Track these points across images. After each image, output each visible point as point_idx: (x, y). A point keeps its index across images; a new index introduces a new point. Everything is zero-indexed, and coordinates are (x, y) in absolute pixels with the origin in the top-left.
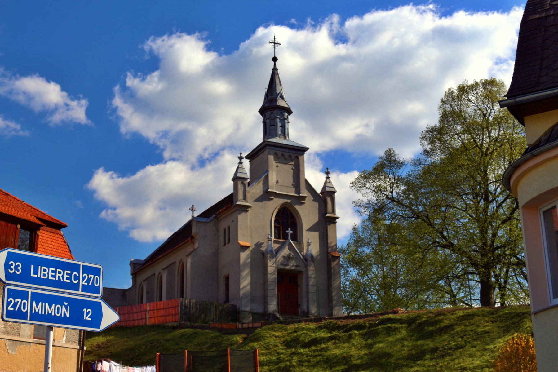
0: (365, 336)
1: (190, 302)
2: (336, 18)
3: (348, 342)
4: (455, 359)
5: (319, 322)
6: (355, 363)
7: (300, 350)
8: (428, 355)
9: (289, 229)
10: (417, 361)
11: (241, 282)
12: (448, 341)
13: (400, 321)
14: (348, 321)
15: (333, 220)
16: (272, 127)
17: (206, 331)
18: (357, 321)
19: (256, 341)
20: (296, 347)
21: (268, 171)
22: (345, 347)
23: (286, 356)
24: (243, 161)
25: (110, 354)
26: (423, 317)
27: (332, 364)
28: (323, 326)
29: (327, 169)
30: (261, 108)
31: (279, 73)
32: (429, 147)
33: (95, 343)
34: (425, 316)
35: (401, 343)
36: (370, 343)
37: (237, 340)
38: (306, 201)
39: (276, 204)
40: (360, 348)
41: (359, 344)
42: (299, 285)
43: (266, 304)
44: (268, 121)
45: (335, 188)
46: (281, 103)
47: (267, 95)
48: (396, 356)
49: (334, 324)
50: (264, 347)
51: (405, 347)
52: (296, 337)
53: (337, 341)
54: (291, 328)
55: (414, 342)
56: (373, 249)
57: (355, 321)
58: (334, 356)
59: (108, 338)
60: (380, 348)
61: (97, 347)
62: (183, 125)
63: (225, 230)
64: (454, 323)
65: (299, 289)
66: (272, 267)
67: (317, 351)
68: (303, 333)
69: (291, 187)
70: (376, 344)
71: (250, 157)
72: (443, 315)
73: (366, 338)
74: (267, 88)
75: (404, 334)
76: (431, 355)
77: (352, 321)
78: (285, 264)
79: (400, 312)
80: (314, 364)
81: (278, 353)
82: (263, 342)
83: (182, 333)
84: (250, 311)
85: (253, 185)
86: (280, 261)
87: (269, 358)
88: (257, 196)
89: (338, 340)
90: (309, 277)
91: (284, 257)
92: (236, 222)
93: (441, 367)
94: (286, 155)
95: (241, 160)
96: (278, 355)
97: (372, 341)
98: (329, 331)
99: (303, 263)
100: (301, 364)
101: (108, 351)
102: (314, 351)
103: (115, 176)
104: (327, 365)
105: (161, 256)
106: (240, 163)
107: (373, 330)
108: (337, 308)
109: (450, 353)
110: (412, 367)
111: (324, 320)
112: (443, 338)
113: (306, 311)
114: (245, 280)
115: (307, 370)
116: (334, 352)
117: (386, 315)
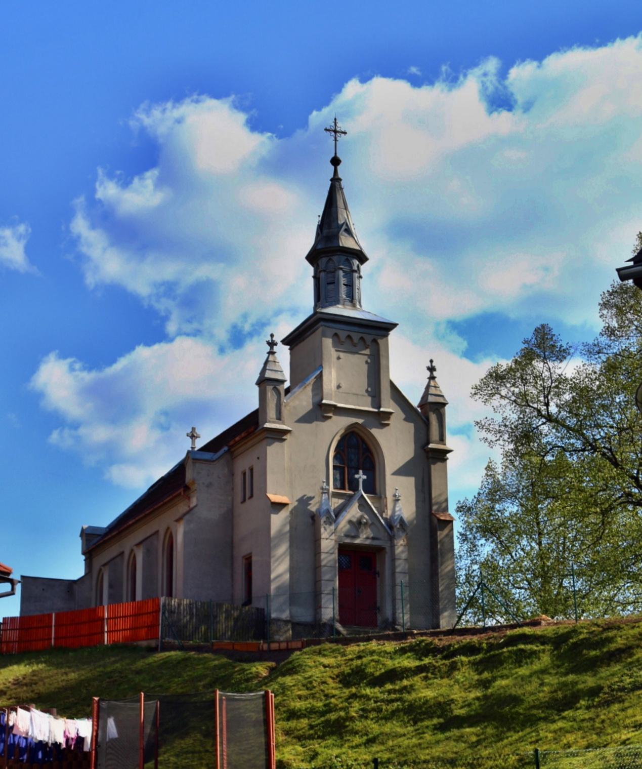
0: (479, 667)
1: (179, 605)
2: (492, 65)
3: (448, 677)
4: (629, 707)
5: (400, 640)
6: (458, 714)
7: (365, 690)
8: (584, 700)
9: (361, 472)
10: (563, 710)
11: (272, 567)
12: (619, 675)
13: (542, 640)
14: (452, 639)
15: (441, 455)
16: (331, 287)
17: (206, 655)
18: (467, 639)
19: (290, 674)
20: (359, 684)
21: (321, 366)
22: (443, 686)
23: (340, 700)
24: (275, 349)
25: (36, 696)
26: (581, 633)
27: (418, 716)
28: (407, 648)
29: (431, 361)
30: (310, 252)
31: (343, 187)
32: (614, 324)
33: (12, 678)
34: (585, 631)
35: (539, 678)
36: (486, 678)
37: (258, 672)
38: (392, 421)
39: (337, 426)
40: (469, 688)
41: (467, 679)
42: (378, 573)
43: (317, 606)
44: (322, 275)
45: (445, 396)
46: (346, 242)
47: (320, 227)
48: (529, 702)
49: (427, 644)
50: (304, 686)
51: (546, 686)
52: (360, 667)
53: (429, 675)
54: (352, 651)
55: (561, 677)
56: (522, 505)
57: (464, 639)
58: (422, 701)
59: (35, 667)
60: (502, 687)
61: (14, 684)
62: (203, 271)
63: (244, 474)
64: (635, 643)
65: (378, 579)
66: (328, 542)
67: (395, 691)
68: (373, 660)
69: (363, 395)
70: (497, 680)
71: (292, 340)
72: (616, 629)
73: (480, 670)
74: (321, 215)
75: (546, 664)
76: (588, 700)
77: (458, 638)
78: (353, 534)
79: (543, 623)
80: (387, 715)
81: (327, 696)
82: (301, 675)
83: (163, 659)
84: (288, 619)
85: (294, 393)
86: (344, 529)
87: (310, 703)
88: (302, 413)
89: (432, 673)
90: (397, 557)
91: (350, 522)
92: (263, 459)
93: (603, 721)
94: (356, 337)
95: (272, 348)
96: (326, 700)
97: (490, 675)
98: (418, 657)
99: (386, 534)
100: (365, 715)
101: (32, 691)
102: (389, 692)
103: (77, 366)
104: (410, 717)
105: (134, 521)
106: (271, 353)
107: (494, 656)
108: (446, 614)
109: (621, 696)
110: (554, 721)
111: (411, 636)
112: (613, 670)
113: (390, 619)
114: (279, 564)
115: (373, 726)
116: (423, 695)
117: (518, 629)
